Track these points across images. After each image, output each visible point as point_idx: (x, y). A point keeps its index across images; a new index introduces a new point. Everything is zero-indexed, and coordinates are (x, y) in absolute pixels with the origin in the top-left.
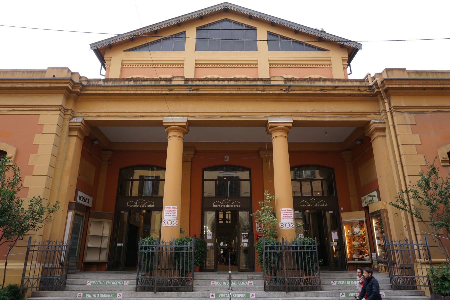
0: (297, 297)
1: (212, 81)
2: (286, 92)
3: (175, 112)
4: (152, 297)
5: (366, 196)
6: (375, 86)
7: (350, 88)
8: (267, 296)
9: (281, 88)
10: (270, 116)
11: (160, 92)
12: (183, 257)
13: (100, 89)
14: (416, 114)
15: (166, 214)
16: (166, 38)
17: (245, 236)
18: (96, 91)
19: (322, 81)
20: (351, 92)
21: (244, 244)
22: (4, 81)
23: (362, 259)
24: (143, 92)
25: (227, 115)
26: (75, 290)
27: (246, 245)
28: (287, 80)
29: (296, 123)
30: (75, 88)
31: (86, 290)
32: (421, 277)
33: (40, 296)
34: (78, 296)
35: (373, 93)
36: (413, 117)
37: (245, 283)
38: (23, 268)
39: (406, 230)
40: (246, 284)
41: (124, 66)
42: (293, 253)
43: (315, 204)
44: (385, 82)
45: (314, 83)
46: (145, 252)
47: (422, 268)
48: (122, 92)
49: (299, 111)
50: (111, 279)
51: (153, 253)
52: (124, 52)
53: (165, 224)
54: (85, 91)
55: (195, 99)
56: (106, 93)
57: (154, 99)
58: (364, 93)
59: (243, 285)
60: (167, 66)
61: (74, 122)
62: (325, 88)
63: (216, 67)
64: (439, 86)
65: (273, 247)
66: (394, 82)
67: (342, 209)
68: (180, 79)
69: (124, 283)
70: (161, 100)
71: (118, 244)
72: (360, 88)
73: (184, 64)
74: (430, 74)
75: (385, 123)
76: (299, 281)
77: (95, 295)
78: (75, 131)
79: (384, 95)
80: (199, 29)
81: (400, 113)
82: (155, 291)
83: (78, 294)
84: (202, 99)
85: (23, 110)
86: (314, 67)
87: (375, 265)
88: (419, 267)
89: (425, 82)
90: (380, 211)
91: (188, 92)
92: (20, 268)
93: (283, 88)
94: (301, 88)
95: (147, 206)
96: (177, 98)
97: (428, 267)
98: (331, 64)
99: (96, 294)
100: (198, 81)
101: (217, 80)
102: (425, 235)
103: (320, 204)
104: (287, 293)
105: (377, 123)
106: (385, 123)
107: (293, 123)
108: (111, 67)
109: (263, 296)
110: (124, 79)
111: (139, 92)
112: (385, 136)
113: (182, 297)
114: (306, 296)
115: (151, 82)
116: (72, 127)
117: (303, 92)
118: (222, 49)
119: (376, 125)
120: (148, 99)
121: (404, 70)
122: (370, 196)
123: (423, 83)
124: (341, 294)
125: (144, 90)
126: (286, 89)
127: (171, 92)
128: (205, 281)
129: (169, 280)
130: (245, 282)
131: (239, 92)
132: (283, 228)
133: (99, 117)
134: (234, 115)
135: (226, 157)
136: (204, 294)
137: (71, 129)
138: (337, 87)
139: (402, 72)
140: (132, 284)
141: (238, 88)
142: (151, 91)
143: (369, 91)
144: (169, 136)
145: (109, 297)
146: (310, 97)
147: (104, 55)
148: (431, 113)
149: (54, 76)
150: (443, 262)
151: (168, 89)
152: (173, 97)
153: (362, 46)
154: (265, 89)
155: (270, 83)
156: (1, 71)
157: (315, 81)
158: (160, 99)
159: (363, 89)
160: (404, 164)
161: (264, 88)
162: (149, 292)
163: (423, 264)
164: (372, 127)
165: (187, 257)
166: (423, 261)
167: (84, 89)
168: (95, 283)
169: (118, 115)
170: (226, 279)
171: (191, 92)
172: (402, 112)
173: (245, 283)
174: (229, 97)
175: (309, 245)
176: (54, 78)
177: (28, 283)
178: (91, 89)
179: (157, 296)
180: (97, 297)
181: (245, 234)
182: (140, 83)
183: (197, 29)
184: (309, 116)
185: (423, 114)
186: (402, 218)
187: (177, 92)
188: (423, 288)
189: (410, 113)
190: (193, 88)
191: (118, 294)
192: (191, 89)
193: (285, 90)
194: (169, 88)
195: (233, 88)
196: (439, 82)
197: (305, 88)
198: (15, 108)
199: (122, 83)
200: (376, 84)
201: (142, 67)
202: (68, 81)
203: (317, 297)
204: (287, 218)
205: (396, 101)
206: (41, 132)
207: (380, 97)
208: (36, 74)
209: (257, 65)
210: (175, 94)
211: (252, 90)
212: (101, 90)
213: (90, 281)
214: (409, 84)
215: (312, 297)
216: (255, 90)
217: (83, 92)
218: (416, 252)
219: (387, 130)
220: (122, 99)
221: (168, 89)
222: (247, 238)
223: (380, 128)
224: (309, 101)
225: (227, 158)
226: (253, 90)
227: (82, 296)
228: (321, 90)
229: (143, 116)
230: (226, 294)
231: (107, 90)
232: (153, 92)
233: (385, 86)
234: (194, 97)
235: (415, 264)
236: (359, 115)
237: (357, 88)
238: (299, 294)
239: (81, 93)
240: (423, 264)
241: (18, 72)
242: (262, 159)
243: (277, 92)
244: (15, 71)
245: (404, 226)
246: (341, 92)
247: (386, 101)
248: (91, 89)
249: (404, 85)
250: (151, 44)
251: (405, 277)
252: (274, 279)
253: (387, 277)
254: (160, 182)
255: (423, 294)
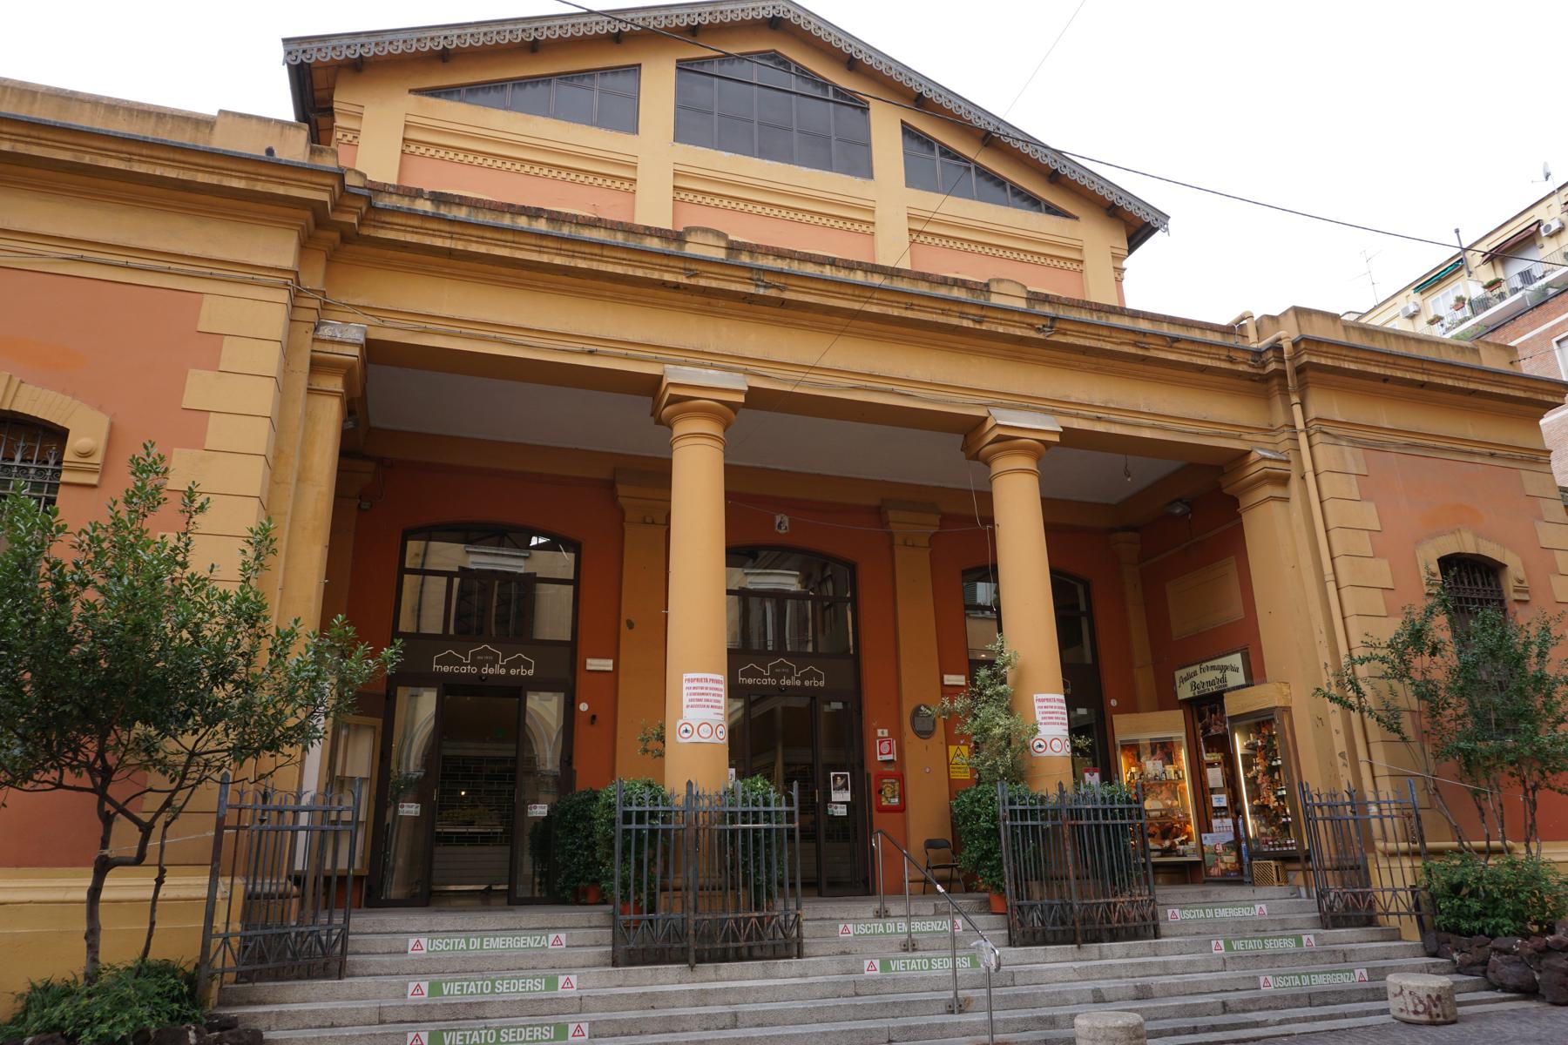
0: (1106, 958)
1: (815, 263)
2: (1041, 336)
3: (703, 352)
4: (680, 983)
5: (1197, 668)
6: (1270, 354)
7: (1208, 350)
8: (1027, 961)
9: (1029, 320)
10: (994, 405)
11: (656, 275)
12: (768, 846)
13: (434, 230)
14: (1368, 446)
15: (691, 700)
16: (566, 77)
17: (840, 782)
18: (416, 233)
19: (1128, 316)
20: (1209, 363)
21: (836, 808)
22: (43, 135)
23: (1170, 851)
24: (595, 266)
25: (868, 384)
26: (379, 972)
27: (841, 811)
28: (1034, 298)
29: (1070, 437)
30: (342, 212)
31: (422, 971)
32: (1401, 890)
33: (255, 999)
34: (410, 992)
35: (1261, 372)
36: (1359, 452)
37: (535, 940)
38: (204, 893)
39: (1345, 765)
40: (539, 943)
41: (413, 148)
42: (1089, 826)
43: (789, 678)
44: (1303, 346)
45: (1107, 317)
46: (638, 831)
47: (1390, 868)
48: (519, 255)
49: (1073, 400)
50: (484, 928)
51: (666, 833)
52: (413, 97)
53: (686, 735)
54: (374, 226)
55: (767, 317)
56: (460, 247)
57: (631, 297)
58: (1241, 368)
59: (934, 931)
60: (573, 176)
61: (332, 342)
62: (1145, 340)
63: (742, 211)
64: (1419, 377)
65: (1031, 810)
66: (1324, 349)
67: (1114, 703)
68: (711, 240)
69: (550, 942)
70: (653, 303)
71: (403, 807)
72: (1232, 354)
73: (635, 180)
74: (1393, 340)
75: (1288, 462)
76: (261, 947)
77: (477, 985)
78: (334, 374)
79: (1291, 382)
80: (683, 67)
81: (1332, 440)
82: (692, 960)
83: (412, 986)
84: (789, 320)
85: (126, 267)
86: (1035, 263)
87: (1211, 867)
88: (1383, 863)
89: (1391, 361)
90: (1270, 711)
91: (752, 290)
92: (71, 896)
93: (1035, 321)
94: (1083, 329)
95: (508, 672)
96: (709, 304)
97: (1418, 863)
98: (1082, 262)
99: (479, 983)
100: (771, 257)
101: (831, 265)
102: (1408, 778)
103: (802, 679)
104: (1079, 948)
105: (1270, 459)
106: (1288, 462)
107: (1060, 433)
108: (361, 139)
109: (1017, 962)
110: (513, 206)
111: (582, 264)
112: (1287, 500)
113: (777, 977)
114: (1128, 956)
115: (612, 233)
116: (323, 359)
117: (1087, 343)
118: (764, 153)
119: (1268, 464)
120: (608, 294)
121: (1335, 317)
122: (1213, 668)
123: (1386, 363)
124: (1214, 943)
125: (601, 258)
126: (1044, 326)
127: (693, 281)
128: (820, 923)
129: (732, 923)
130: (538, 938)
131: (909, 314)
132: (1044, 754)
133: (425, 332)
134: (890, 387)
135: (778, 519)
136: (844, 962)
137: (318, 366)
138: (1177, 340)
139: (1329, 323)
140: (578, 943)
141: (909, 301)
142: (625, 268)
143: (1253, 366)
144: (675, 436)
145: (529, 991)
146: (1102, 361)
147: (334, 88)
148: (1399, 448)
149: (270, 151)
150: (1447, 849)
151: (685, 269)
152: (696, 298)
153: (1170, 221)
154: (985, 317)
155: (989, 300)
156: (6, 87)
157: (1110, 313)
158: (650, 300)
159: (1239, 356)
160: (1343, 582)
161: (984, 313)
162: (670, 966)
163: (1393, 855)
164: (1254, 471)
165: (652, 845)
166: (1391, 846)
167: (371, 220)
168: (440, 944)
169: (498, 335)
170: (871, 915)
171: (761, 291)
172: (1335, 437)
173: (535, 940)
174: (875, 326)
175: (1126, 806)
176: (271, 159)
177: (224, 952)
178: (397, 224)
179: (698, 979)
180: (482, 992)
181: (840, 775)
182: (573, 229)
183: (677, 68)
184: (1099, 419)
185: (1379, 447)
186: (1334, 733)
187: (714, 284)
188: (1393, 920)
189: (1352, 441)
190: (767, 279)
191: (562, 980)
192: (763, 281)
193: (1039, 329)
194: (688, 266)
195: (892, 298)
196: (1420, 366)
197: (1093, 331)
198: (86, 254)
199: (506, 221)
200: (1276, 348)
201: (480, 165)
202: (329, 181)
203: (1156, 955)
204: (1054, 724)
205: (1324, 405)
206: (213, 365)
207: (1277, 388)
208: (169, 127)
209: (871, 227)
210: (706, 291)
211: (947, 315)
212: (440, 236)
213: (560, 935)
214: (1356, 360)
215: (1143, 955)
216: (956, 317)
217: (365, 231)
218: (1375, 823)
219: (1294, 483)
220: (512, 280)
221: (685, 269)
222: (847, 789)
223: (1277, 474)
224: (1098, 371)
225: (783, 521)
226: (951, 316)
227: (426, 991)
228: (1135, 344)
229: (591, 352)
230: (911, 959)
231: (460, 239)
232: (630, 272)
233: (1300, 356)
234: (766, 309)
235: (1370, 856)
236: (1224, 430)
237: (1225, 352)
238: (1110, 948)
239: (358, 234)
240: (1393, 855)
241: (88, 106)
242: (891, 535)
243: (1018, 332)
244: (70, 99)
245: (1338, 752)
246: (1185, 359)
247: (1295, 399)
248: (397, 224)
249: (1344, 360)
250: (514, 85)
251: (1358, 890)
252: (646, 923)
253: (1289, 895)
254: (539, 586)
255: (1395, 935)
